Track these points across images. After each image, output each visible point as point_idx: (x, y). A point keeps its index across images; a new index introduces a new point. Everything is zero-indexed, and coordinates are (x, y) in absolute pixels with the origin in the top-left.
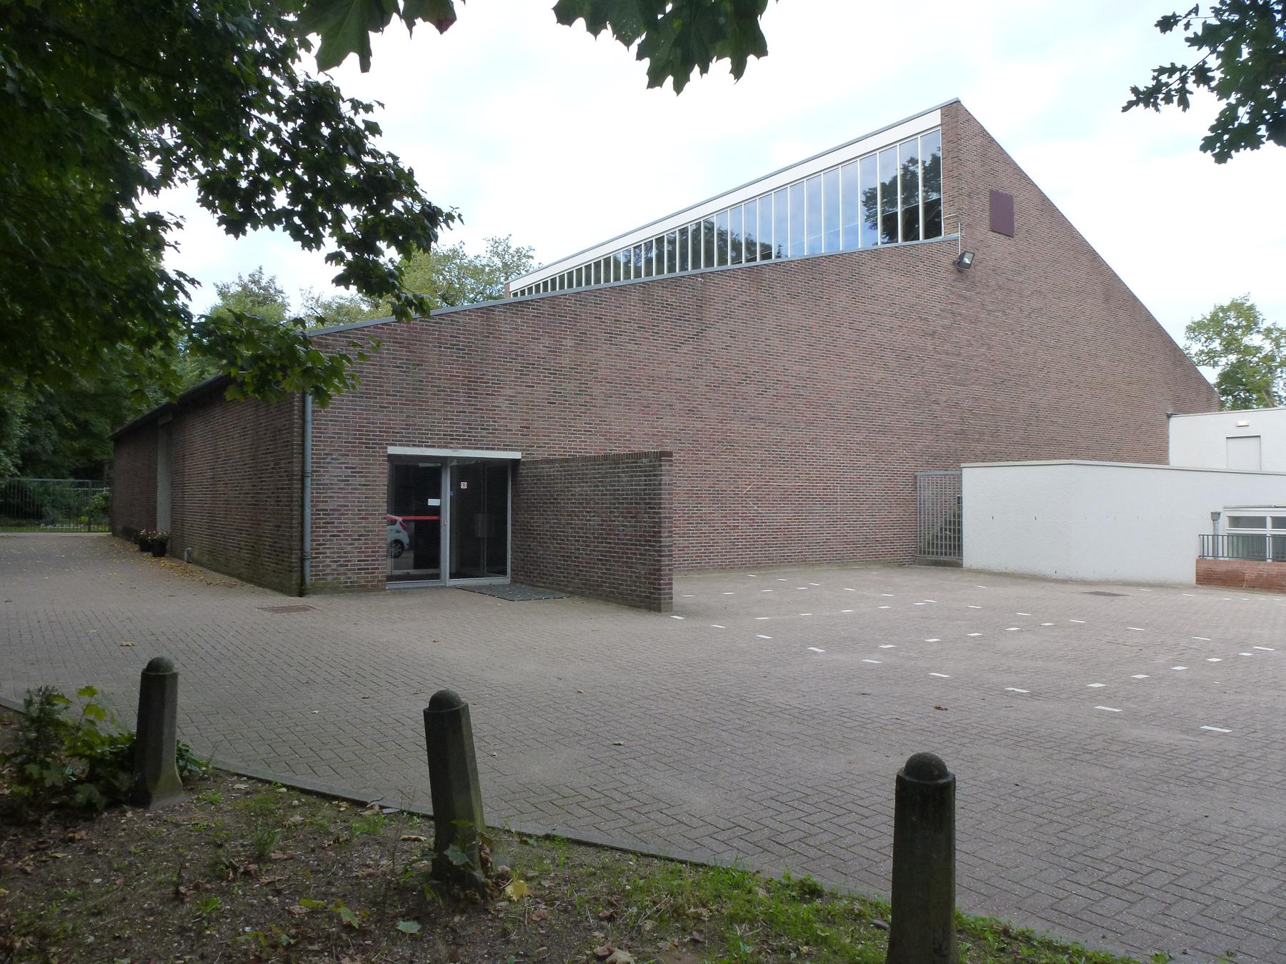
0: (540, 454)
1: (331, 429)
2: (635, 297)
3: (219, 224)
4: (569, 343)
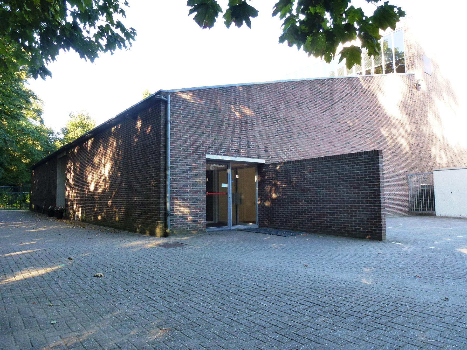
0: (273, 161)
1: (179, 144)
2: (307, 87)
3: (45, 72)
4: (283, 106)
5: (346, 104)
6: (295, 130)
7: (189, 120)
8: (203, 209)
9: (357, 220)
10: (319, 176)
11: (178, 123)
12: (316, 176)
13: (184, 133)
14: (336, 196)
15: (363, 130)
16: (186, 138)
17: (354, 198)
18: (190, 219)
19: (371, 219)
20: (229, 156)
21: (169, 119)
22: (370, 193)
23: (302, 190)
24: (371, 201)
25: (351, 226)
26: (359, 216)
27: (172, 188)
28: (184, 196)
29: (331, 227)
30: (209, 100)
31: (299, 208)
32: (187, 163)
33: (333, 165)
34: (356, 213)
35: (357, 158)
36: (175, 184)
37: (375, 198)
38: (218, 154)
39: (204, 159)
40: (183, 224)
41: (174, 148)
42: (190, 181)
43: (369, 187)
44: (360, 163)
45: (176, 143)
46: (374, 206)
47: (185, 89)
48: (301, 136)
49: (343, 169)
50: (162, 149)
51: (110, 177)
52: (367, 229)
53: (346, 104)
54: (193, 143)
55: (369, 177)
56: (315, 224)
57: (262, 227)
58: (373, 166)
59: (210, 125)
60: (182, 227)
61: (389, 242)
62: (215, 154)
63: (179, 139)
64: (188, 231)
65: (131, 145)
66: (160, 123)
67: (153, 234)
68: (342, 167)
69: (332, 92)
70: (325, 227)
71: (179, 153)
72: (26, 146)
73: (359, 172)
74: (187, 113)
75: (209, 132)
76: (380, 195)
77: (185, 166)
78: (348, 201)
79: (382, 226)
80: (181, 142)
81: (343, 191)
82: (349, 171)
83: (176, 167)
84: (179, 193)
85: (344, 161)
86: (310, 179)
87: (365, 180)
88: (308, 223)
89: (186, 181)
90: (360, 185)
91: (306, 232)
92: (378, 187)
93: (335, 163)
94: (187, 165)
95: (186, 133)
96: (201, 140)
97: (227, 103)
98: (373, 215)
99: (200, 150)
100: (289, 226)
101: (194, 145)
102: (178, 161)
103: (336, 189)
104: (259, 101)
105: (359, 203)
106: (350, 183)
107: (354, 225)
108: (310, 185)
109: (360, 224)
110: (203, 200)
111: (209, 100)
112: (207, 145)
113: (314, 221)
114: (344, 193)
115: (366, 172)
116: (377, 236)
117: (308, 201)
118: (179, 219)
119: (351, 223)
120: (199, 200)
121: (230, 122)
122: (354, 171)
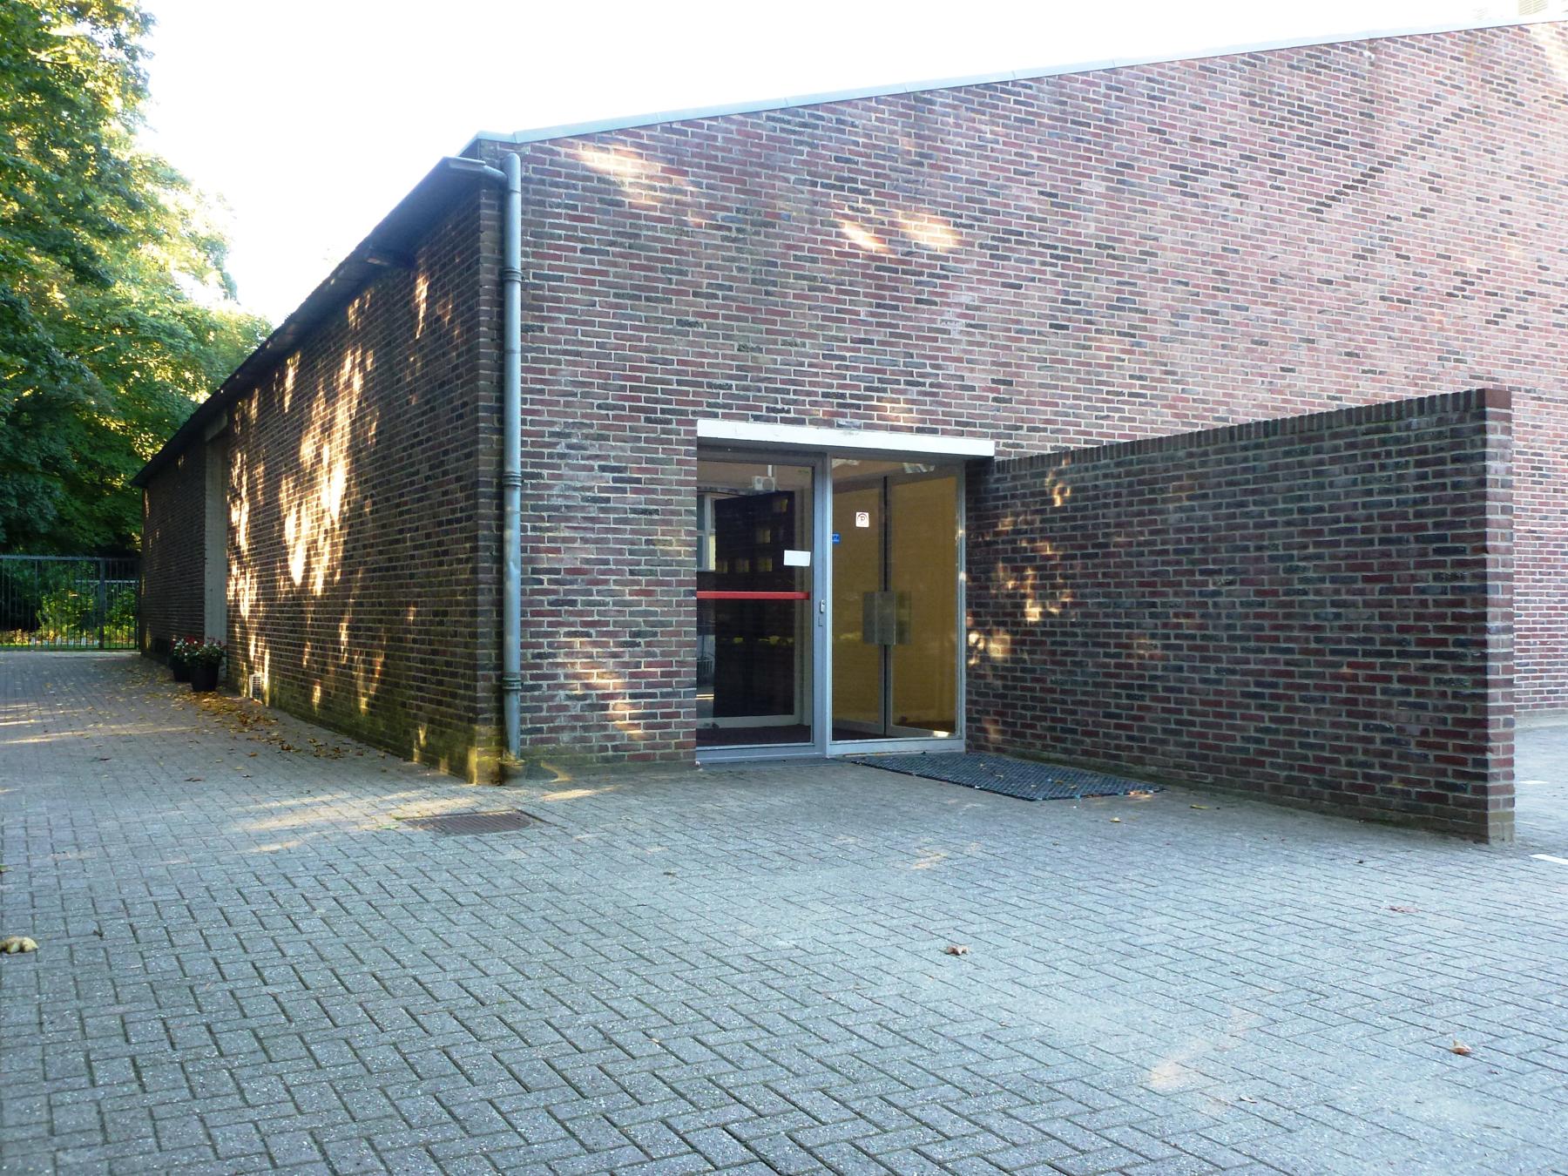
1: (566, 374)
4: (1095, 186)
5: (1448, 166)
6: (1155, 299)
7: (615, 265)
8: (681, 664)
9: (1378, 736)
10: (1216, 518)
11: (560, 279)
12: (1204, 518)
13: (592, 324)
14: (1287, 616)
15: (1544, 289)
16: (599, 345)
17: (1366, 629)
18: (621, 709)
19: (1438, 733)
20: (816, 422)
21: (517, 261)
22: (1437, 603)
23: (1141, 584)
24: (1444, 643)
25: (1349, 763)
26: (1385, 717)
27: (535, 571)
28: (590, 603)
29: (1262, 764)
30: (716, 168)
31: (1130, 666)
32: (606, 458)
33: (1275, 467)
34: (1371, 703)
35: (1387, 430)
36: (549, 550)
37: (1463, 630)
38: (757, 418)
39: (689, 443)
40: (586, 729)
41: (541, 392)
42: (617, 541)
43: (1437, 577)
44: (1400, 453)
45: (552, 372)
46: (1457, 669)
47: (535, 131)
48: (1190, 325)
49: (1321, 486)
50: (486, 399)
51: (343, 520)
52: (1421, 783)
53: (1448, 166)
54: (632, 368)
55: (1437, 525)
56: (1191, 745)
57: (980, 748)
58: (1458, 472)
59: (720, 287)
60: (583, 740)
61: (1527, 848)
62: (744, 418)
63: (566, 352)
64: (606, 760)
65: (399, 381)
66: (477, 282)
67: (460, 772)
68: (1317, 474)
69: (1370, 108)
70: (1234, 761)
71: (566, 415)
72: (148, 390)
73: (1393, 498)
74: (605, 233)
75: (715, 316)
76: (1483, 617)
77: (597, 473)
78: (1339, 641)
79: (1493, 770)
80: (575, 364)
81: (1318, 592)
82: (1347, 495)
83: (552, 477)
84: (567, 592)
85: (1327, 444)
86: (1179, 531)
87: (1418, 540)
88: (1164, 742)
89: (596, 541)
90: (1394, 566)
91: (1159, 781)
92: (1475, 576)
93: (1287, 454)
94: (603, 469)
95: (601, 325)
96: (676, 353)
97: (803, 182)
98: (1449, 716)
99: (669, 402)
100: (1085, 753)
101: (638, 379)
102: (561, 449)
103: (1288, 582)
104: (969, 168)
105: (1389, 654)
106: (1348, 556)
107: (1361, 757)
108: (1179, 563)
109: (1388, 754)
110: (680, 624)
111: (716, 168)
112: (705, 375)
113: (1190, 734)
114: (1322, 604)
115: (1424, 501)
116: (1465, 817)
117: (1167, 637)
118: (566, 708)
119: (1351, 750)
120: (662, 624)
121: (819, 270)
122: (1370, 493)
